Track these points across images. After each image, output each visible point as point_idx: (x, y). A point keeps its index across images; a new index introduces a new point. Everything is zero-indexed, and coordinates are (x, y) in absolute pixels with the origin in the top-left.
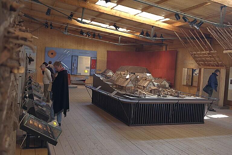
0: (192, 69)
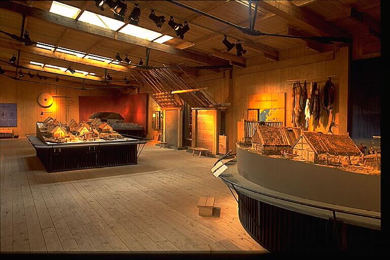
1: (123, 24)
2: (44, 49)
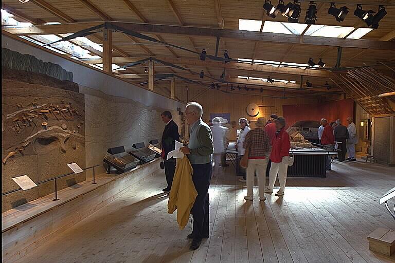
0: (367, 121)
1: (353, 29)
2: (244, 62)
